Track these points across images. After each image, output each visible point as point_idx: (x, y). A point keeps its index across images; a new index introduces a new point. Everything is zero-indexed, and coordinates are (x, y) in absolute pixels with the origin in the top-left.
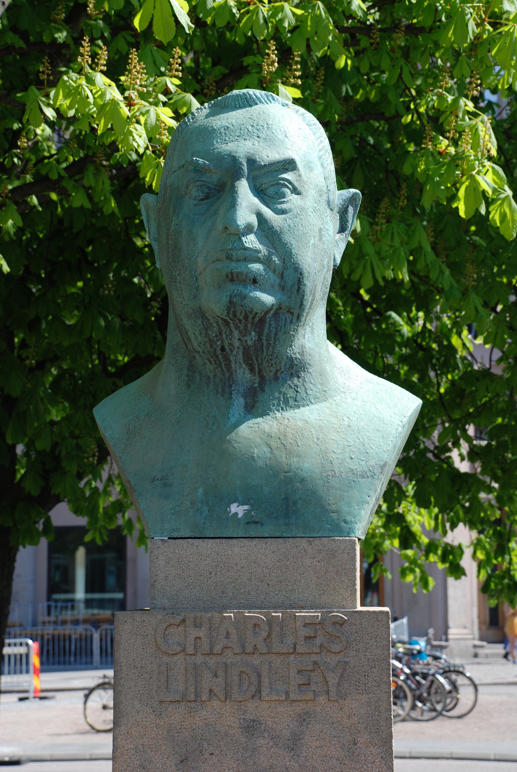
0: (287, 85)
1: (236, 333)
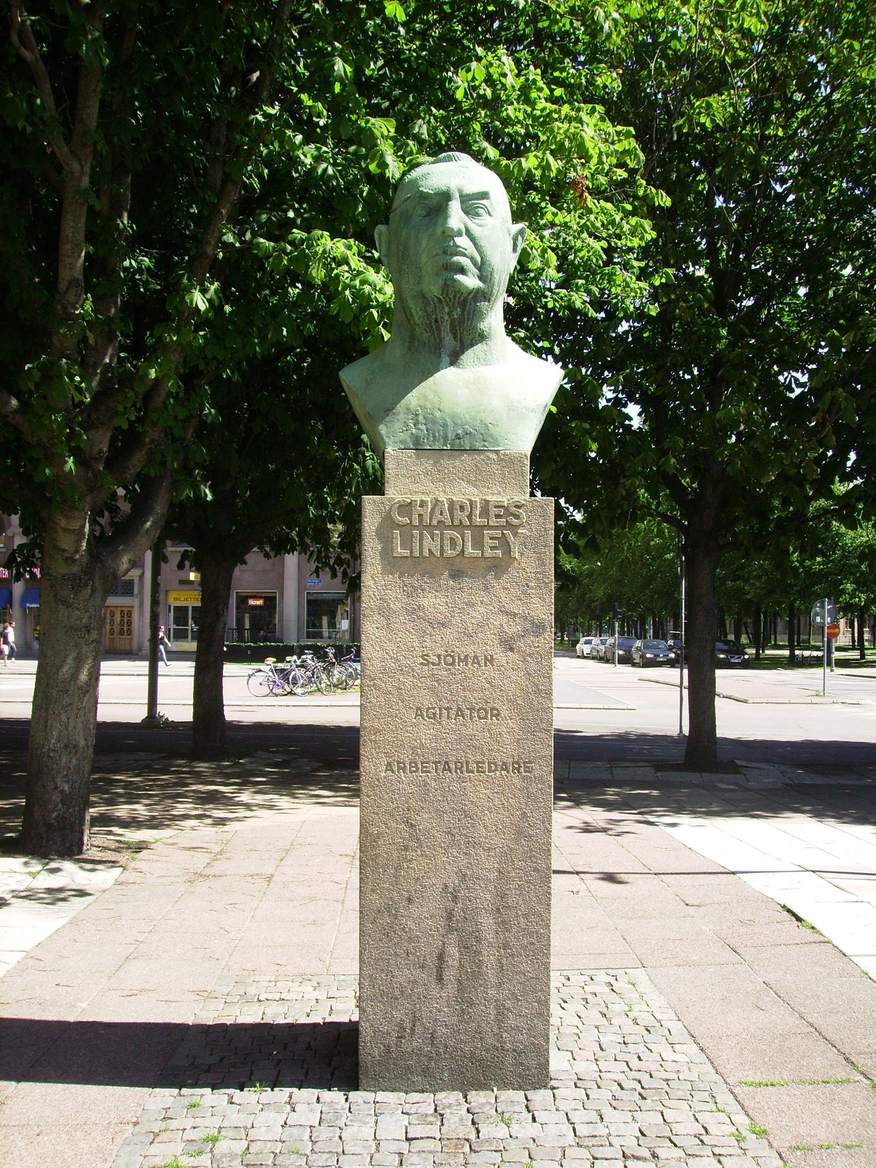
0: (478, 161)
1: (446, 309)
